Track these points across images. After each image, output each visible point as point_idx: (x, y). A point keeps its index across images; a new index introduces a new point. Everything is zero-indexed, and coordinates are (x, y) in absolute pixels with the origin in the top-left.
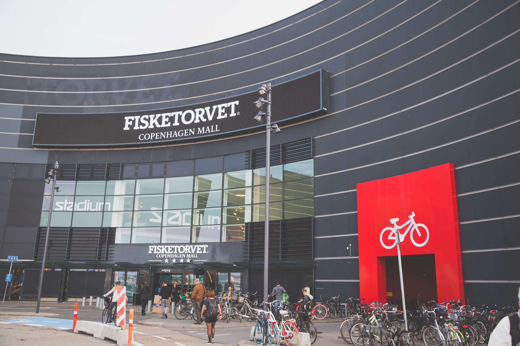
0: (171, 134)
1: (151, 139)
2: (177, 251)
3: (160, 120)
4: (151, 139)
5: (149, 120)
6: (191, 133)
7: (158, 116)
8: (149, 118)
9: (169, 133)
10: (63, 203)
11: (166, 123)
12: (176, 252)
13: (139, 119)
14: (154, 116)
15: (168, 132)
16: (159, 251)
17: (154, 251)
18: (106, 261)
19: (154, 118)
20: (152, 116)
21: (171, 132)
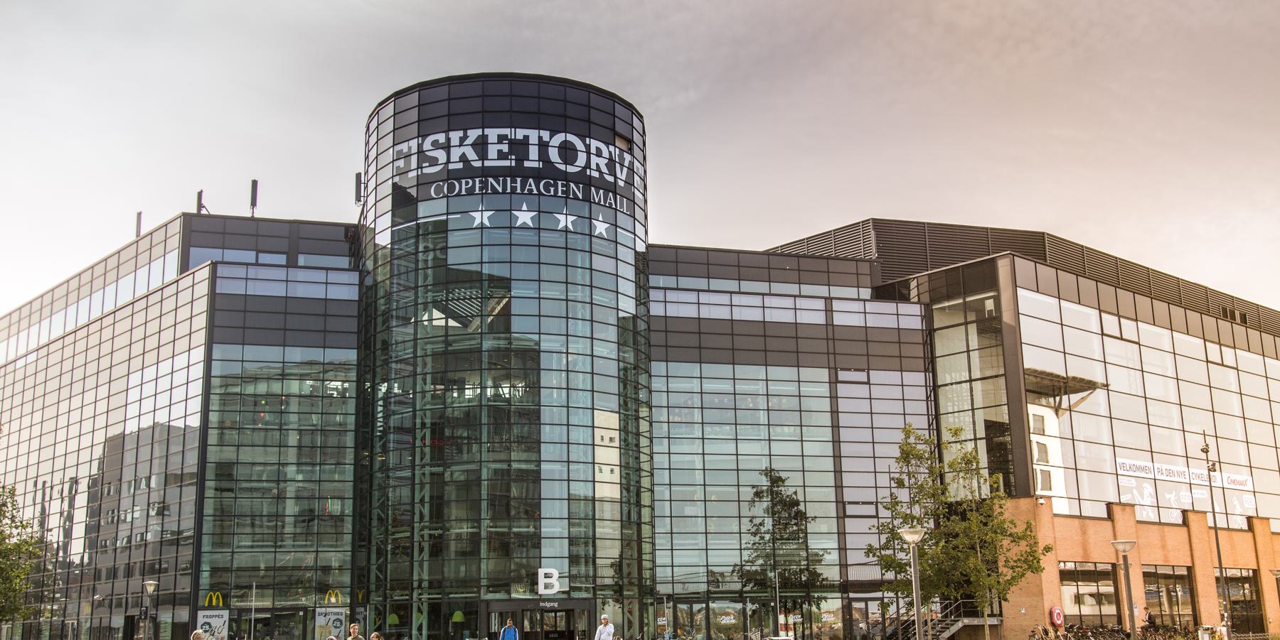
2: (543, 156)
3: (481, 146)
5: (447, 147)
6: (574, 192)
7: (474, 134)
8: (448, 140)
9: (514, 181)
11: (501, 156)
12: (533, 162)
14: (461, 133)
16: (436, 145)
19: (462, 140)
20: (455, 136)
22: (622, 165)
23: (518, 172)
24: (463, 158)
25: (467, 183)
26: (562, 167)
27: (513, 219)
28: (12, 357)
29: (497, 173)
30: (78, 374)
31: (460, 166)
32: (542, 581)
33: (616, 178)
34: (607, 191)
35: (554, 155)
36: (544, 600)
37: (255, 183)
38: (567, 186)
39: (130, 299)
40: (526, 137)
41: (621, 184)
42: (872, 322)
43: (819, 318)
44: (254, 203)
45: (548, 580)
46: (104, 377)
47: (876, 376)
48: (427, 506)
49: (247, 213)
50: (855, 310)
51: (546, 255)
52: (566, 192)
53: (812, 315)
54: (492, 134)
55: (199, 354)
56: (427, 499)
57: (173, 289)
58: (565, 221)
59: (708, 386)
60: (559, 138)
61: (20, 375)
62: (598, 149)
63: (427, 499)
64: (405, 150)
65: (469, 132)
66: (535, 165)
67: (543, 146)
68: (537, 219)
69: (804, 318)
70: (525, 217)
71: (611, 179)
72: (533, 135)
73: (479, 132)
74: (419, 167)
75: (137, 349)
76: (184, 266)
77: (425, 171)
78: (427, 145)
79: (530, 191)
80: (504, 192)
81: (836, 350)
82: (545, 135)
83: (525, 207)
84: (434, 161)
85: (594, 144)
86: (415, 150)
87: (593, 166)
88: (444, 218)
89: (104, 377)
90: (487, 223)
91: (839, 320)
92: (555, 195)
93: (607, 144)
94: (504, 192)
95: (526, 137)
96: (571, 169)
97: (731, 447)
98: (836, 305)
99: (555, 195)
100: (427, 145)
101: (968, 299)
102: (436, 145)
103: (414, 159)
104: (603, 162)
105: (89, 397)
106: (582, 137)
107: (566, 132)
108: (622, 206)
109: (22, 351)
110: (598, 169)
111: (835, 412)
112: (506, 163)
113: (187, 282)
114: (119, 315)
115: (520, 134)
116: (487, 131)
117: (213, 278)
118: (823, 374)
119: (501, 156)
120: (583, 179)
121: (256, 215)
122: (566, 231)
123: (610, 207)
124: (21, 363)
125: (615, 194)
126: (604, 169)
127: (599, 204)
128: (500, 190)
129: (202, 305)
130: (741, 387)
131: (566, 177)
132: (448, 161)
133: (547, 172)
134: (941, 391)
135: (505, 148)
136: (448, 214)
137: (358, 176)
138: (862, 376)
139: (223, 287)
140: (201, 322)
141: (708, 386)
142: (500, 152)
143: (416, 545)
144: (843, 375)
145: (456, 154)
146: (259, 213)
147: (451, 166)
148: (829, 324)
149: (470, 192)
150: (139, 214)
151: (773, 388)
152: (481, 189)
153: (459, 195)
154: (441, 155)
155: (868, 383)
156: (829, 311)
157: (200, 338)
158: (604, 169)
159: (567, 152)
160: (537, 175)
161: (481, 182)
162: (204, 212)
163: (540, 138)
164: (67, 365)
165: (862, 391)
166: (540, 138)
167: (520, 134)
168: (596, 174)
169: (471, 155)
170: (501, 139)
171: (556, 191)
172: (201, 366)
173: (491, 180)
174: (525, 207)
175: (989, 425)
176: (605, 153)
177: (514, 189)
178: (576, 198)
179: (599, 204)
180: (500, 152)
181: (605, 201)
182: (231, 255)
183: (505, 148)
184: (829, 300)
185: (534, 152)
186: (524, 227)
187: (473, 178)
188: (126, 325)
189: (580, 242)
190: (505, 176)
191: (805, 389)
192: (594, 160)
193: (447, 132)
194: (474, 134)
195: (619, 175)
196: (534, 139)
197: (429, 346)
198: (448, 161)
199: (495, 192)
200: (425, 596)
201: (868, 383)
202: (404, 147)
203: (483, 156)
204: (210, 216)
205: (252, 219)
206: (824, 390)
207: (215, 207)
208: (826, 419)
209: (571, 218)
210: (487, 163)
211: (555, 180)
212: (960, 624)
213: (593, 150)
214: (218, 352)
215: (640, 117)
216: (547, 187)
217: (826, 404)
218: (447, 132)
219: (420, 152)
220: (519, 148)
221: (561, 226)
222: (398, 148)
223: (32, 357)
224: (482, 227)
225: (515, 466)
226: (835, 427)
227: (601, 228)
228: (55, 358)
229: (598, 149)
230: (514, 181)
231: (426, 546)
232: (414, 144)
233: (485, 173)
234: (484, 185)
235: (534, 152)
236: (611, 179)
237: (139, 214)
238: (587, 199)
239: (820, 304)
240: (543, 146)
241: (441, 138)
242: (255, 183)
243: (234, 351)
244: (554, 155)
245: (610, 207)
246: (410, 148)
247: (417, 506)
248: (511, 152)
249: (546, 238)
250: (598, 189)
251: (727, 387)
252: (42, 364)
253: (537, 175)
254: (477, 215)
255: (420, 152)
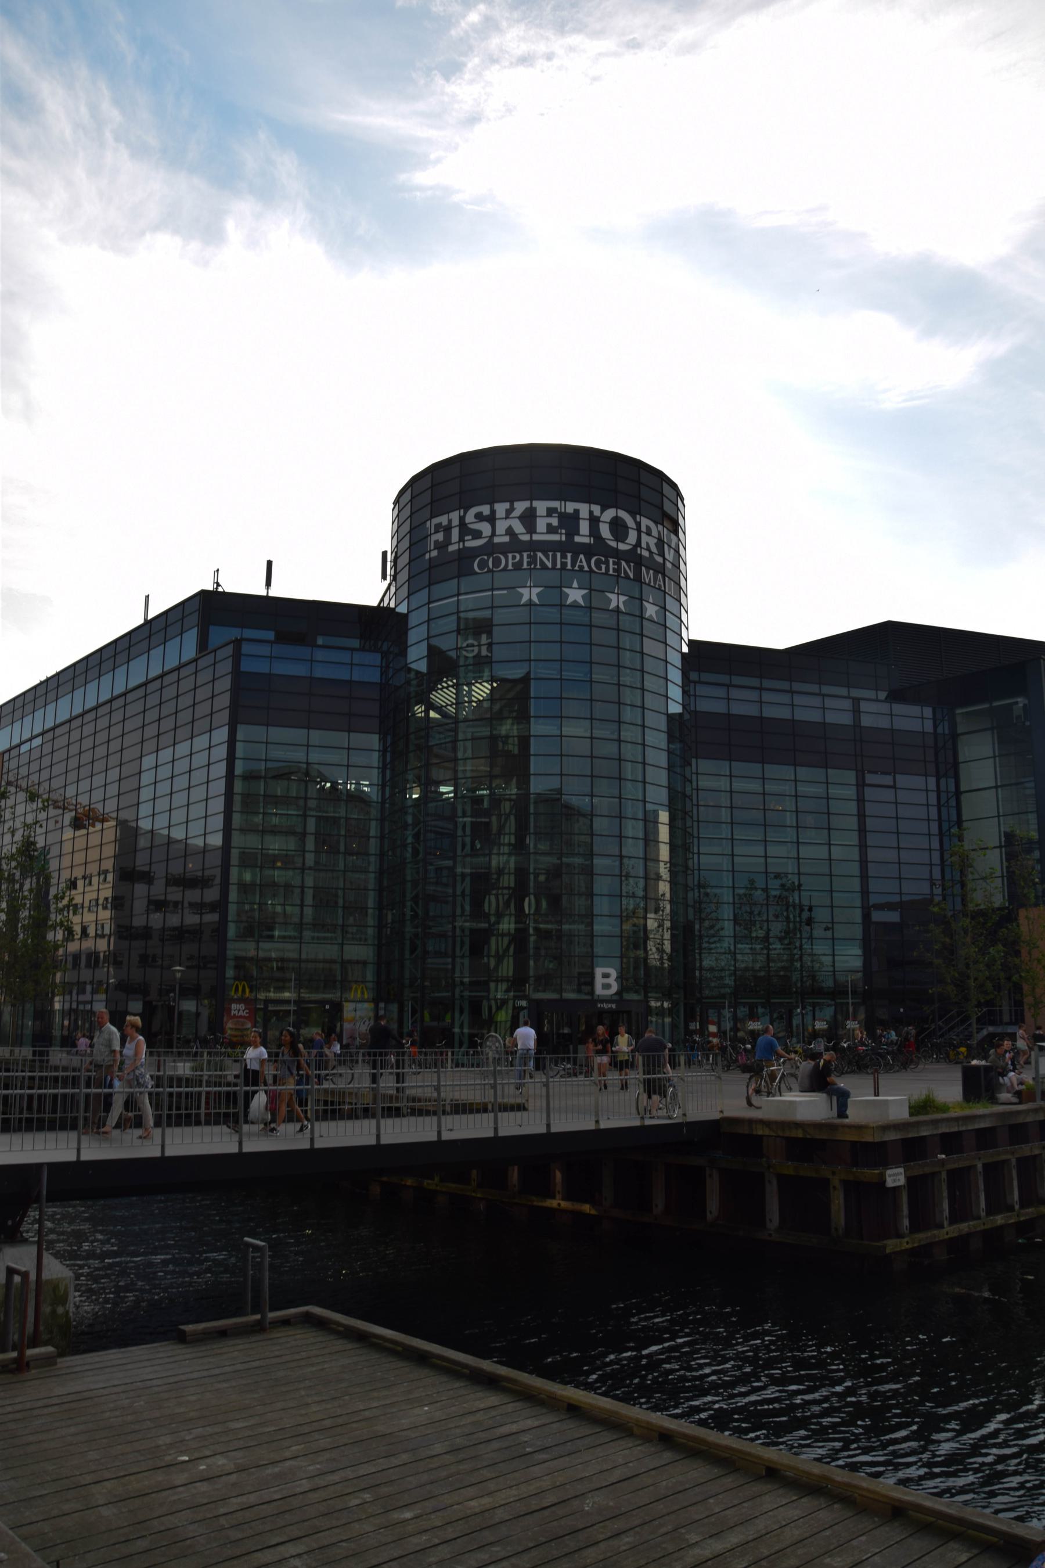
0: (569, 561)
1: (510, 567)
2: (594, 531)
3: (529, 519)
4: (510, 567)
5: (492, 519)
6: (625, 572)
7: (521, 506)
8: (493, 512)
9: (563, 556)
10: (469, 813)
11: (551, 529)
12: (583, 536)
13: (462, 519)
14: (507, 505)
15: (559, 555)
16: (479, 517)
17: (447, 541)
18: (238, 643)
19: (509, 512)
20: (501, 508)
21: (569, 555)
22: (669, 546)
23: (569, 547)
24: (510, 531)
25: (514, 558)
26: (613, 544)
27: (564, 596)
28: (16, 741)
29: (545, 547)
30: (86, 757)
31: (507, 539)
32: (599, 981)
33: (664, 559)
34: (656, 572)
35: (605, 531)
36: (602, 1001)
37: (270, 564)
38: (618, 564)
39: (67, 717)
40: (577, 511)
41: (669, 565)
42: (900, 724)
43: (846, 719)
44: (268, 583)
45: (606, 981)
46: (114, 760)
47: (902, 780)
48: (468, 899)
49: (262, 592)
50: (877, 712)
51: (598, 636)
52: (617, 570)
53: (839, 715)
54: (541, 507)
55: (221, 735)
56: (467, 892)
57: (191, 668)
58: (616, 600)
59: (738, 785)
60: (610, 514)
61: (24, 759)
62: (648, 527)
63: (467, 892)
64: (445, 523)
65: (517, 504)
66: (586, 540)
67: (594, 521)
68: (587, 598)
69: (831, 718)
70: (575, 595)
71: (660, 560)
72: (584, 509)
73: (526, 504)
74: (461, 539)
75: (73, 763)
76: (203, 645)
77: (467, 544)
78: (470, 517)
79: (581, 567)
80: (554, 567)
81: (862, 753)
82: (596, 509)
83: (575, 585)
84: (477, 534)
85: (645, 522)
86: (456, 522)
87: (644, 545)
88: (487, 613)
89: (114, 760)
90: (535, 599)
91: (866, 721)
92: (607, 573)
93: (656, 523)
94: (554, 567)
95: (577, 511)
96: (622, 547)
97: (759, 850)
98: (864, 706)
99: (607, 573)
100: (470, 517)
101: (995, 704)
102: (479, 517)
103: (455, 534)
104: (652, 542)
105: (98, 780)
106: (633, 514)
107: (617, 508)
108: (670, 590)
109: (26, 735)
110: (648, 549)
111: (862, 816)
112: (555, 537)
113: (208, 660)
114: (58, 732)
115: (570, 507)
116: (535, 504)
117: (237, 657)
118: (850, 777)
119: (551, 529)
120: (633, 556)
121: (270, 594)
122: (617, 610)
123: (659, 589)
124: (25, 748)
125: (664, 576)
126: (654, 549)
127: (649, 585)
128: (550, 565)
129: (225, 684)
130: (770, 787)
131: (616, 554)
132: (494, 534)
133: (597, 548)
134: (964, 798)
135: (555, 522)
136: (492, 590)
137: (385, 554)
138: (888, 780)
139: (246, 666)
140: (225, 700)
141: (738, 785)
142: (549, 525)
143: (458, 939)
144: (870, 778)
145: (501, 526)
146: (274, 592)
147: (496, 540)
148: (857, 725)
149: (518, 566)
150: (147, 597)
151: (802, 789)
152: (529, 564)
153: (505, 569)
154: (485, 528)
155: (894, 787)
156: (856, 712)
157: (224, 716)
158: (654, 549)
159: (618, 528)
160: (588, 551)
161: (529, 556)
162: (220, 589)
163: (591, 513)
164: (74, 749)
165: (888, 795)
166: (591, 513)
167: (570, 507)
168: (645, 553)
169: (519, 528)
170: (550, 512)
171: (607, 569)
172: (224, 748)
173: (539, 554)
174: (575, 585)
175: (1009, 838)
176: (655, 533)
177: (564, 564)
178: (627, 577)
179: (649, 585)
180: (549, 525)
181: (655, 583)
182: (249, 633)
183: (555, 522)
184: (856, 701)
185: (584, 527)
186: (575, 605)
187: (520, 552)
188: (138, 707)
189: (626, 622)
190: (554, 551)
191: (833, 791)
192: (645, 538)
193: (491, 504)
194: (521, 506)
195: (667, 556)
196: (584, 513)
197: (471, 730)
198: (494, 534)
199: (544, 567)
200: (466, 993)
201: (894, 787)
202: (443, 520)
203: (531, 529)
204: (224, 593)
205: (267, 598)
206: (851, 792)
207: (229, 586)
208: (853, 822)
209: (622, 598)
210: (535, 537)
211: (606, 557)
212: (985, 1032)
213: (643, 529)
214: (242, 732)
215: (682, 500)
216: (598, 564)
217: (852, 807)
218: (491, 504)
219: (462, 524)
220: (570, 522)
221: (613, 605)
222: (436, 521)
223: (37, 742)
224: (530, 604)
225: (947, 732)
226: (862, 831)
227: (651, 610)
228: (61, 742)
229: (648, 527)
230: (563, 556)
231: (467, 940)
232: (455, 516)
233: (534, 547)
234: (533, 560)
235: (584, 527)
236: (660, 560)
237: (147, 597)
238: (638, 578)
239: (847, 704)
240: (594, 521)
241: (485, 510)
242: (270, 564)
243: (258, 732)
244: (605, 531)
245: (659, 589)
246: (450, 521)
247: (459, 899)
248: (561, 525)
249: (598, 618)
250: (648, 568)
251: (755, 786)
252: (47, 748)
253: (588, 551)
254: (525, 592)
255: (462, 524)
